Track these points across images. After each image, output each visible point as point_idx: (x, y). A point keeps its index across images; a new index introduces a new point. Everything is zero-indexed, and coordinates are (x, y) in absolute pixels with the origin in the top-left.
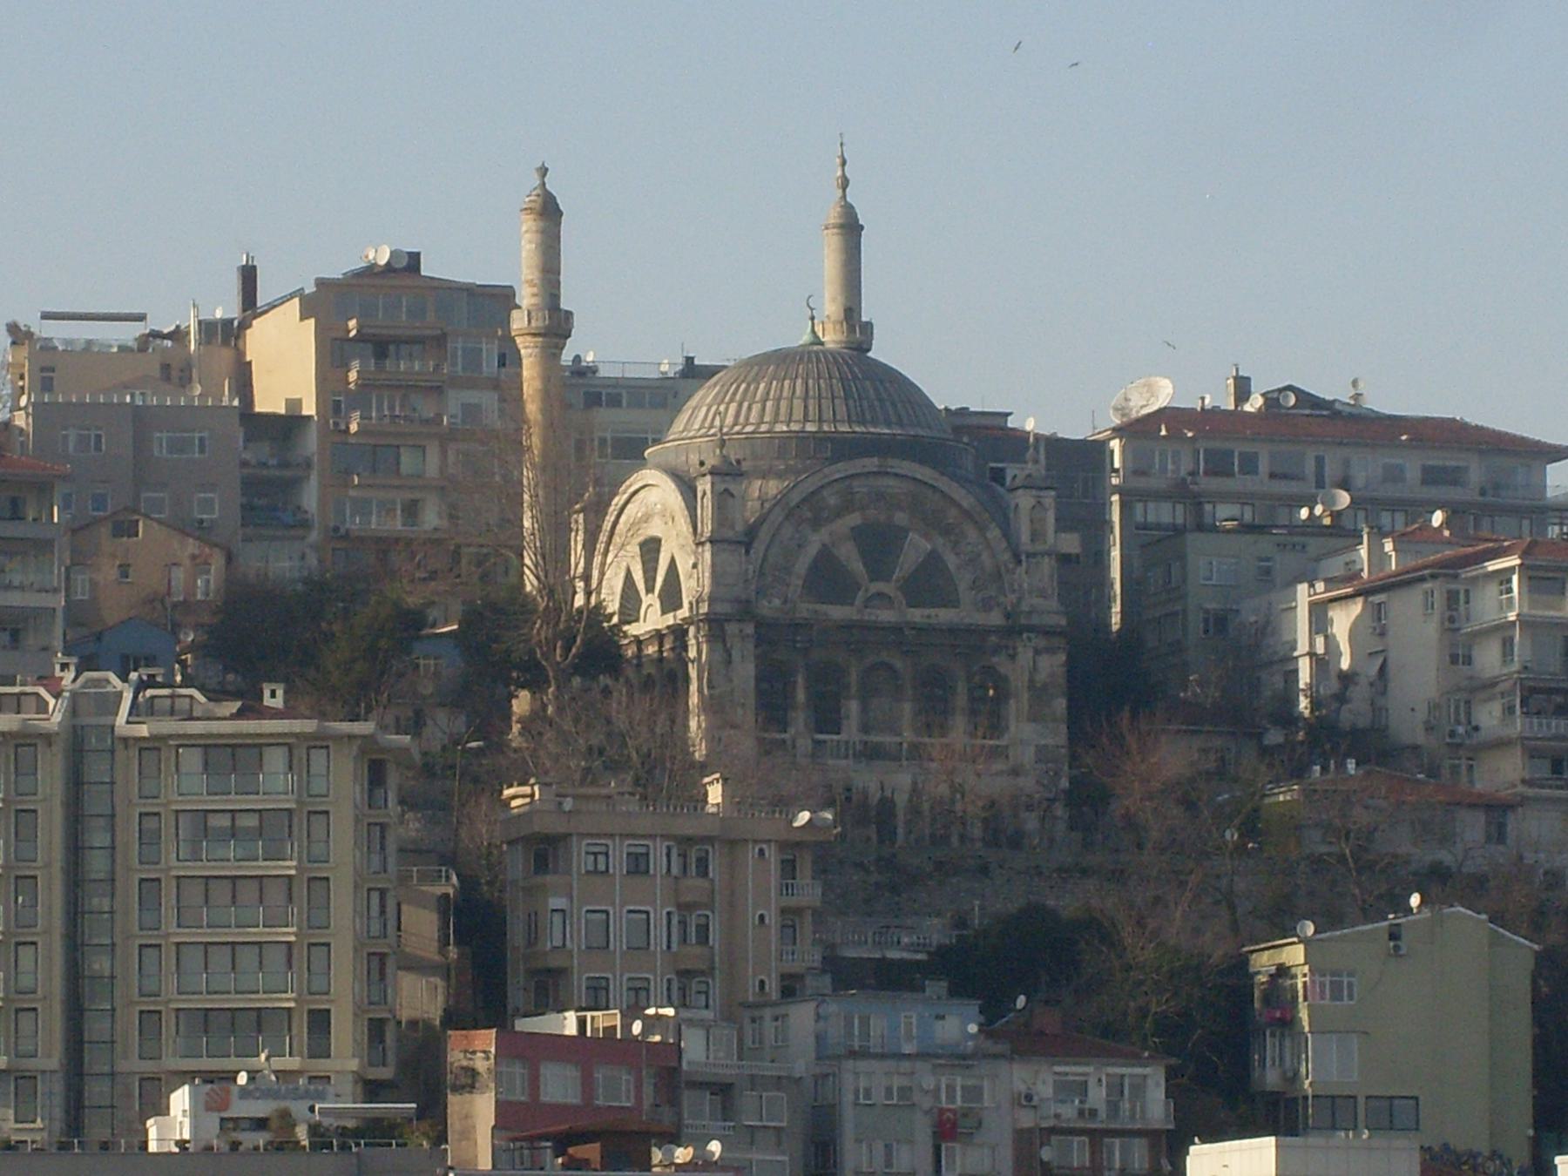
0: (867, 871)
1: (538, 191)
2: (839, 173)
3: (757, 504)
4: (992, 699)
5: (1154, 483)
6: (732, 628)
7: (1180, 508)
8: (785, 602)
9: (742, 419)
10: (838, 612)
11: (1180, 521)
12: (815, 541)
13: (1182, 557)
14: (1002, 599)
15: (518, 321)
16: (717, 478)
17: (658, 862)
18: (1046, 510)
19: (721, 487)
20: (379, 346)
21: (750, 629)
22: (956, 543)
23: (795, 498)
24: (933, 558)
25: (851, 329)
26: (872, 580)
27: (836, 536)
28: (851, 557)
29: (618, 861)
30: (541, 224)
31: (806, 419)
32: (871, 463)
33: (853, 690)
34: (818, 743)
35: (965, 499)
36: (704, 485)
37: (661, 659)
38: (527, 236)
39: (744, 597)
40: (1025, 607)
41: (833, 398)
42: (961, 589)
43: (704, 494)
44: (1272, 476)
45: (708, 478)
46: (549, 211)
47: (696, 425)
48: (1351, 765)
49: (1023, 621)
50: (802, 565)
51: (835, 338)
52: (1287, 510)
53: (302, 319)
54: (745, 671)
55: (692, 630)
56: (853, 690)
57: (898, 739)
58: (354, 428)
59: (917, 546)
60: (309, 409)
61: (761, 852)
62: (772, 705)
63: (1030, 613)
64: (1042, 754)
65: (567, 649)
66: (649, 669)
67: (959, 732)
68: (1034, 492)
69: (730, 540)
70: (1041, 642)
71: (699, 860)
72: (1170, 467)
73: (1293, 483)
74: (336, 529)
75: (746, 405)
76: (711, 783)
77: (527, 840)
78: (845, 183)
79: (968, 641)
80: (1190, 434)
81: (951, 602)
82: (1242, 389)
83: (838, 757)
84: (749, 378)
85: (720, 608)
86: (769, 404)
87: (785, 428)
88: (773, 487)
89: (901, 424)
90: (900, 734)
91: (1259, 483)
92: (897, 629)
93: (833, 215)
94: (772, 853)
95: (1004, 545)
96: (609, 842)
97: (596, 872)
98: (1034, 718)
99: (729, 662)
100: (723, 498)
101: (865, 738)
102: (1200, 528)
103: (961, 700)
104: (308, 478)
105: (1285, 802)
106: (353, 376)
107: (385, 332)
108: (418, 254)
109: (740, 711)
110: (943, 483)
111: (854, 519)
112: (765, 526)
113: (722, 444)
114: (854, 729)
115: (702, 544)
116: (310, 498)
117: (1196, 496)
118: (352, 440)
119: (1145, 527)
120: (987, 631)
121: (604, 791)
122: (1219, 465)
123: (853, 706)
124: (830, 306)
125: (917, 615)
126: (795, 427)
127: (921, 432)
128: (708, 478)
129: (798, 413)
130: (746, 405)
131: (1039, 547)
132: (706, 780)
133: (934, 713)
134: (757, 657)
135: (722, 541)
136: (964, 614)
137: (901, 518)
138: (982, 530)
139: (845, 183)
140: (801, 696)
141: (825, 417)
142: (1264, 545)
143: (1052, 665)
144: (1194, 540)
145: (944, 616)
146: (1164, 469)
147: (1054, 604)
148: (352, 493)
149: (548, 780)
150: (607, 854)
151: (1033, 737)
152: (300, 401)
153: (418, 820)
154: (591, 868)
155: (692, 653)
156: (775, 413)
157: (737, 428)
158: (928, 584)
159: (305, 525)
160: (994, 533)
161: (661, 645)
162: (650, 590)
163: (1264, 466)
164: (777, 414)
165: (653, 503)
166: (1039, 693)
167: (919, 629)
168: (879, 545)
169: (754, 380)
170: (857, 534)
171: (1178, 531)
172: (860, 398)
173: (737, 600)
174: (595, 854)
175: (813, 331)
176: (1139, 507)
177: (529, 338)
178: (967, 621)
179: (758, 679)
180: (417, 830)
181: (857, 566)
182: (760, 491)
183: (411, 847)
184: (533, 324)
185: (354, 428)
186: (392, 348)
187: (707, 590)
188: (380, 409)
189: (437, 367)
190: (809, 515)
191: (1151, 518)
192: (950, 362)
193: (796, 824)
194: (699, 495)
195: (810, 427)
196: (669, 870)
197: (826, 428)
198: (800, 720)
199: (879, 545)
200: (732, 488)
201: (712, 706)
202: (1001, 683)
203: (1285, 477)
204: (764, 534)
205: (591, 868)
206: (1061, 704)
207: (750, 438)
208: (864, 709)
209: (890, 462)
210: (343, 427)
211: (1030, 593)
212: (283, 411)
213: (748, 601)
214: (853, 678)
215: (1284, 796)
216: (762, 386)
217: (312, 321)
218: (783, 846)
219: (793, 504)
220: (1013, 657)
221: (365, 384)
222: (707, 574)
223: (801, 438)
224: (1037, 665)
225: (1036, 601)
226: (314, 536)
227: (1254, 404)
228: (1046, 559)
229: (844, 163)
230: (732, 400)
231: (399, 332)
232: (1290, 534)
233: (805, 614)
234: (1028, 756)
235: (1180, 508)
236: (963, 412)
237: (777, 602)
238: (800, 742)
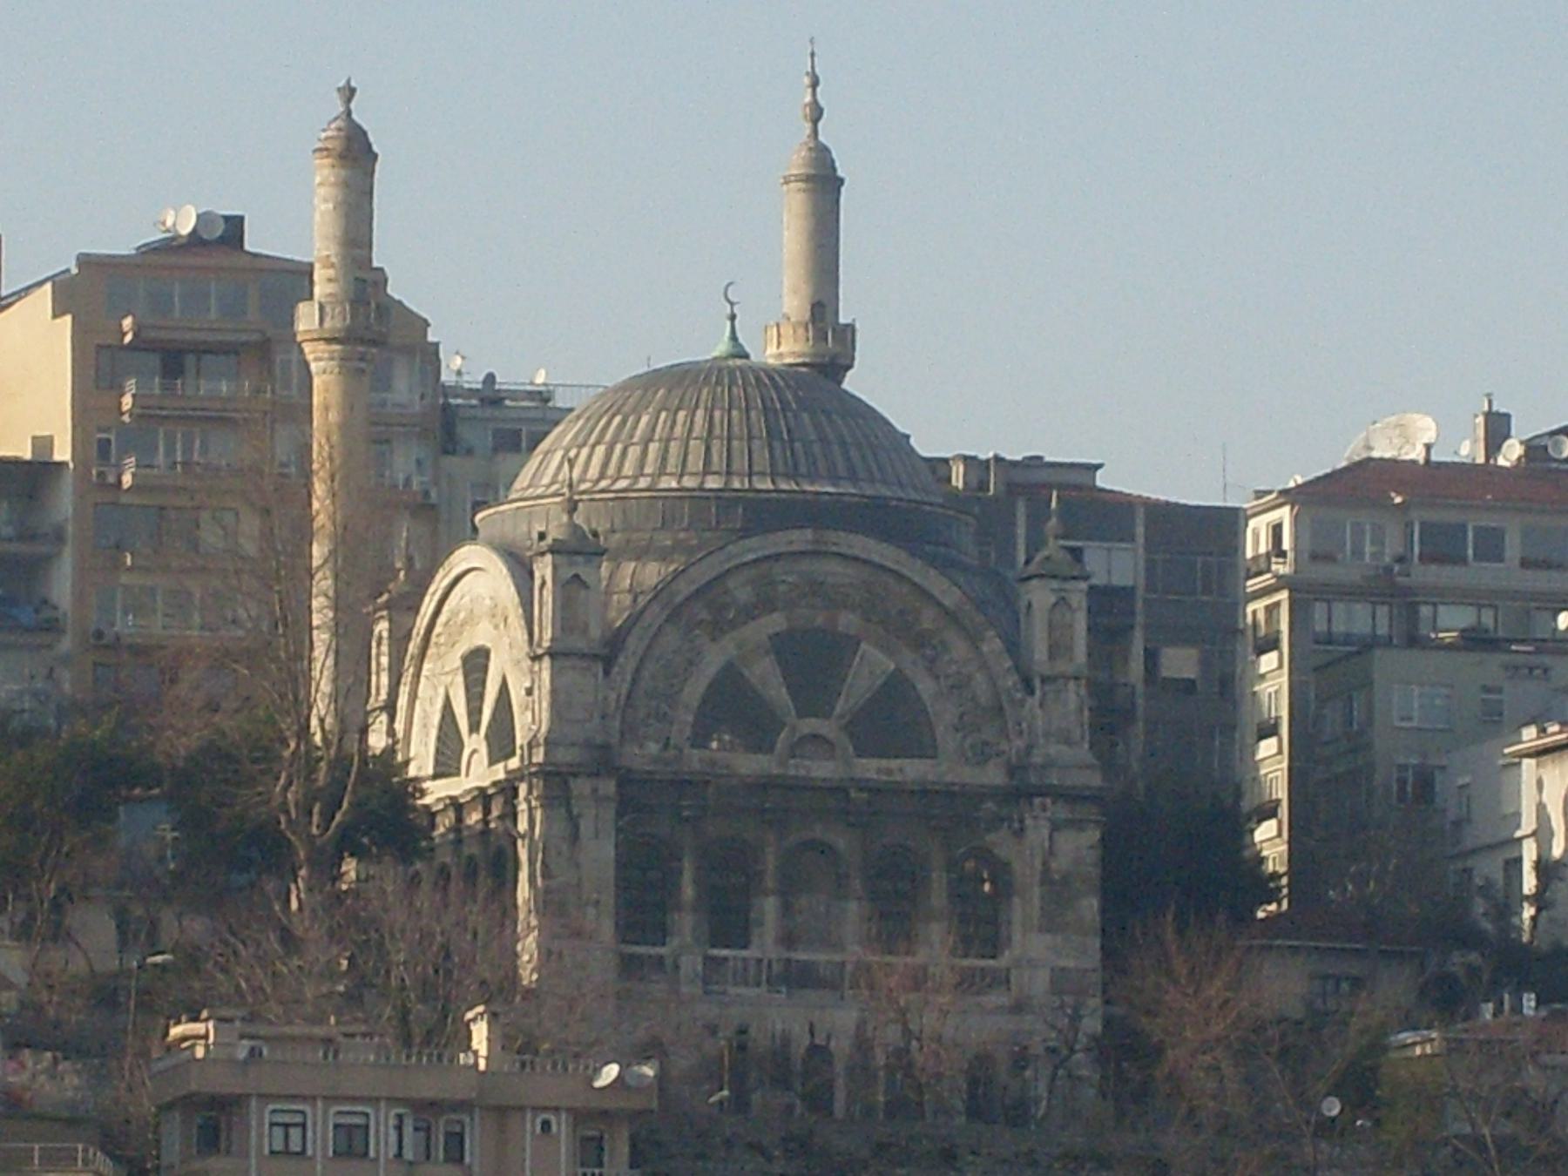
0: (770, 1159)
1: (339, 123)
2: (808, 99)
3: (627, 599)
4: (988, 897)
5: (1344, 572)
6: (581, 786)
7: (1382, 611)
8: (666, 746)
9: (611, 471)
10: (912, 770)
11: (1382, 630)
12: (714, 659)
13: (1367, 684)
14: (1004, 746)
15: (306, 319)
16: (560, 559)
17: (382, 1141)
18: (1073, 611)
19: (568, 573)
20: (172, 359)
21: (609, 787)
22: (933, 661)
23: (684, 589)
24: (895, 688)
25: (821, 336)
26: (801, 715)
27: (750, 648)
28: (768, 679)
29: (321, 1139)
30: (343, 173)
31: (707, 472)
32: (800, 538)
33: (770, 883)
34: (708, 960)
35: (947, 592)
36: (544, 569)
37: (485, 832)
38: (322, 191)
39: (599, 740)
40: (1037, 759)
41: (750, 438)
42: (940, 730)
43: (543, 583)
44: (1525, 563)
45: (549, 558)
46: (355, 153)
47: (541, 480)
48: (1529, 1002)
49: (1033, 780)
50: (694, 691)
51: (797, 348)
52: (1325, 605)
53: (55, 316)
54: (600, 852)
55: (523, 789)
56: (770, 883)
57: (837, 958)
58: (127, 480)
59: (872, 664)
60: (62, 452)
61: (546, 1125)
62: (642, 908)
63: (1043, 767)
64: (1060, 981)
65: (328, 817)
66: (472, 849)
67: (935, 946)
68: (1055, 584)
69: (577, 651)
70: (1062, 812)
71: (448, 1135)
72: (1368, 549)
73: (1555, 574)
74: (99, 635)
75: (619, 448)
76: (474, 1020)
77: (189, 1103)
78: (816, 113)
79: (950, 810)
80: (1398, 500)
81: (926, 750)
82: (1497, 428)
83: (746, 984)
84: (626, 409)
85: (564, 756)
86: (653, 447)
87: (674, 484)
88: (653, 573)
89: (853, 477)
90: (843, 949)
91: (1506, 574)
92: (837, 790)
93: (796, 161)
94: (561, 1126)
95: (1008, 664)
96: (308, 1109)
97: (287, 1152)
98: (1050, 924)
99: (575, 837)
100: (570, 588)
101: (786, 955)
102: (1413, 641)
103: (938, 898)
104: (59, 554)
105: (1424, 1056)
106: (127, 402)
107: (176, 335)
108: (241, 219)
109: (591, 911)
110: (916, 570)
111: (776, 622)
112: (636, 631)
113: (572, 507)
114: (769, 939)
115: (536, 658)
116: (62, 586)
117: (1407, 591)
118: (124, 499)
119: (1329, 639)
120: (982, 794)
121: (318, 1031)
122: (1442, 546)
123: (769, 906)
124: (793, 302)
125: (869, 768)
126: (689, 482)
127: (885, 492)
128: (549, 558)
129: (696, 462)
130: (619, 448)
131: (1062, 667)
132: (470, 1015)
133: (895, 919)
134: (619, 830)
135: (566, 655)
136: (945, 767)
137: (848, 621)
138: (974, 640)
139: (816, 113)
140: (688, 892)
141: (735, 466)
142: (1491, 666)
143: (1079, 847)
144: (1385, 663)
145: (912, 770)
146: (1358, 552)
147: (1083, 752)
148: (124, 579)
149: (225, 1013)
150: (304, 1126)
151: (1047, 952)
152: (51, 438)
153: (78, 1072)
154: (278, 1146)
155: (522, 826)
156: (670, 460)
157: (603, 484)
158: (891, 721)
159: (52, 627)
160: (992, 644)
161: (487, 811)
162: (474, 727)
163: (1513, 548)
164: (664, 459)
165: (480, 597)
166: (1058, 890)
167: (876, 790)
168: (813, 662)
169: (634, 410)
170: (781, 646)
171: (1369, 644)
172: (792, 441)
173: (588, 744)
174: (287, 1126)
175: (734, 337)
176: (1319, 610)
177: (322, 346)
178: (949, 778)
179: (621, 864)
180: (76, 1089)
181: (778, 693)
182: (629, 580)
183: (66, 1114)
184: (327, 324)
185: (127, 480)
186: (190, 360)
187: (544, 729)
188: (170, 451)
189: (258, 391)
190: (704, 615)
191: (1339, 627)
192: (951, 390)
193: (599, 1084)
194: (537, 583)
195: (713, 483)
196: (399, 1155)
197: (736, 485)
198: (685, 925)
199: (813, 662)
200: (584, 572)
201: (548, 903)
202: (1001, 872)
203: (1546, 565)
204: (634, 644)
205: (278, 1146)
206: (1090, 906)
207: (621, 498)
208: (787, 909)
209: (831, 536)
210: (111, 479)
211: (1047, 735)
212: (28, 456)
213: (605, 747)
214: (771, 861)
215: (1420, 1044)
216: (645, 419)
217: (68, 318)
218: (580, 1117)
219: (679, 599)
220: (1020, 833)
221: (146, 414)
222: (545, 705)
223: (698, 497)
224: (1057, 848)
225: (1053, 750)
226: (66, 644)
227: (1511, 453)
228: (1072, 685)
229: (815, 84)
230: (598, 443)
231: (201, 336)
232: (1538, 652)
233: (697, 766)
234: (1039, 984)
235: (1382, 611)
236: (1035, 462)
237: (653, 748)
238: (685, 961)
